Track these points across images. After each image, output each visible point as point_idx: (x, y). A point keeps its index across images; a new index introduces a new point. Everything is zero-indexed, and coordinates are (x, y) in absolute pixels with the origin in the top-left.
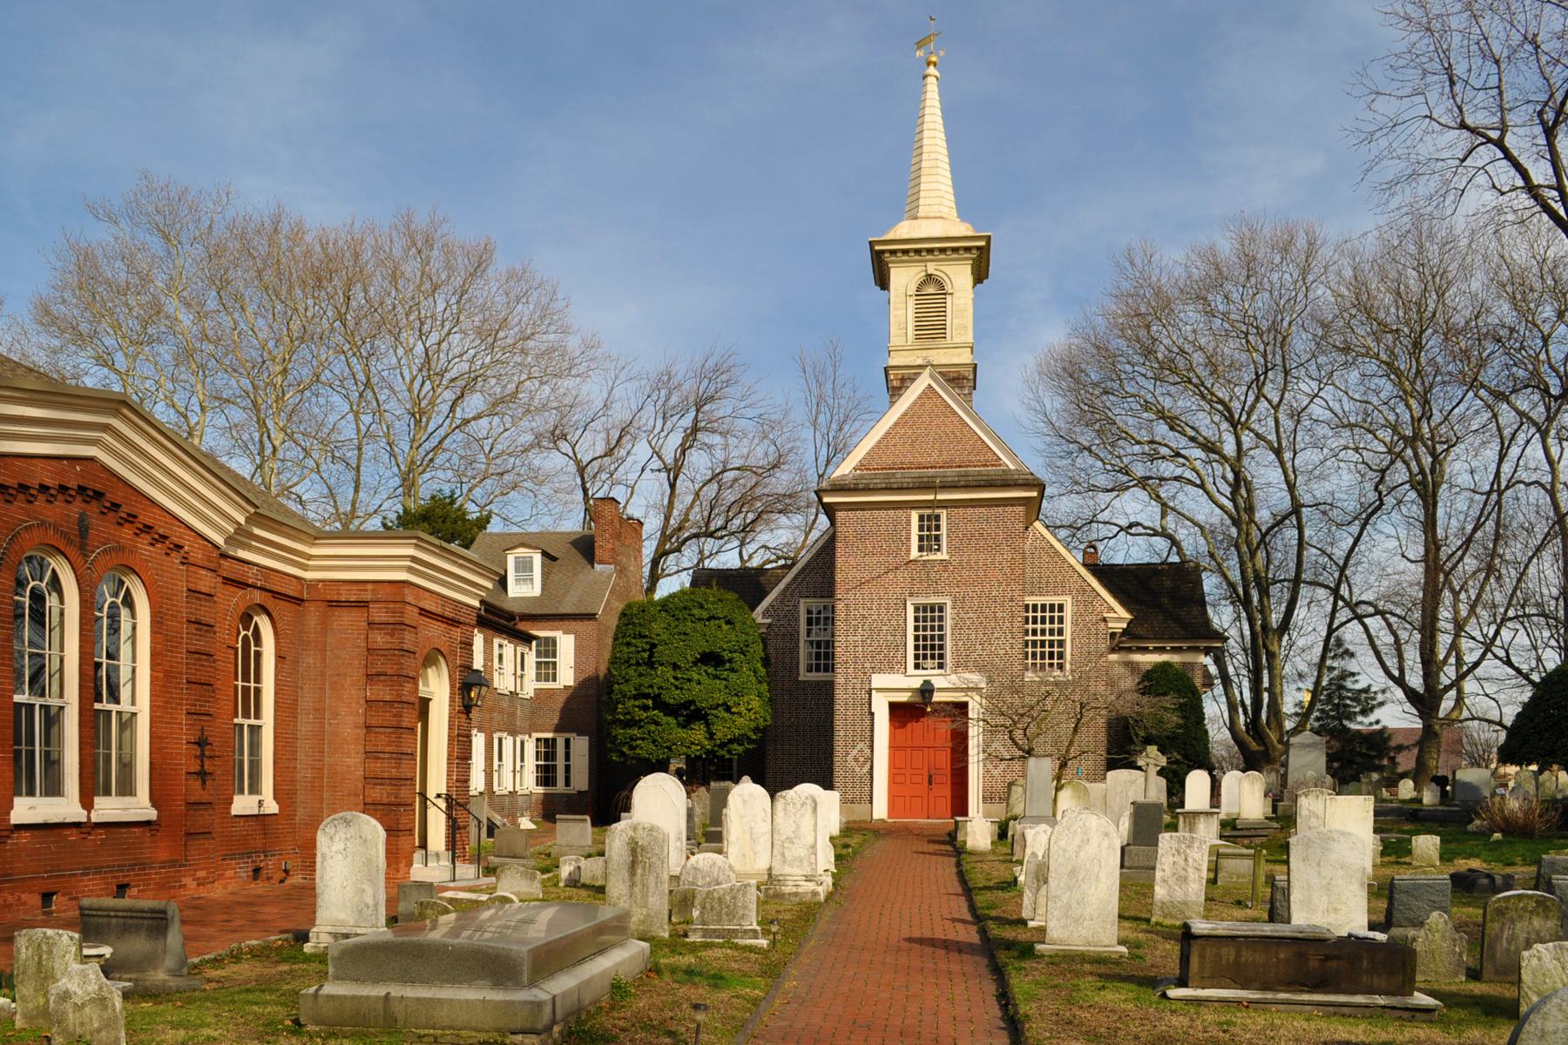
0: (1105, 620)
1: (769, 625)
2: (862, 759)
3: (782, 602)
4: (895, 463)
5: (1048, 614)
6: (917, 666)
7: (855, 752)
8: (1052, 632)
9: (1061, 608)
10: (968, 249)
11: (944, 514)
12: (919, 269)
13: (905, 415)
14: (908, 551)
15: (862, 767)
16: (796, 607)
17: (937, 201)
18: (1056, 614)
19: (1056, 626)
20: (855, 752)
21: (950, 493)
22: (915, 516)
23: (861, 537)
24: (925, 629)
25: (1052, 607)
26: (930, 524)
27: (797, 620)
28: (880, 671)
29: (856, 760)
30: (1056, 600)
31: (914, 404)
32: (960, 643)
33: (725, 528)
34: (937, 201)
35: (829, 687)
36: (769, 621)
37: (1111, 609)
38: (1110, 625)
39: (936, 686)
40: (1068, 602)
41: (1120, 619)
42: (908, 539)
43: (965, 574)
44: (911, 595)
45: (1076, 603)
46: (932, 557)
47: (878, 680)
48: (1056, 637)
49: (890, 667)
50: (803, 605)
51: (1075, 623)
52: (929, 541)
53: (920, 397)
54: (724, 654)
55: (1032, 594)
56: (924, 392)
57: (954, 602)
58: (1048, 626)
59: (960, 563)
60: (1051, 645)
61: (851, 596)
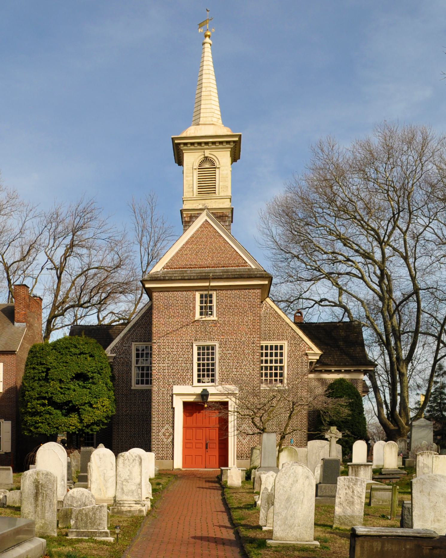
0: (306, 354)
1: (115, 358)
2: (167, 434)
3: (122, 344)
4: (186, 265)
5: (274, 351)
6: (199, 381)
7: (163, 430)
8: (276, 362)
9: (281, 348)
10: (228, 142)
11: (214, 294)
12: (200, 154)
13: (192, 237)
14: (194, 315)
15: (167, 439)
16: (130, 347)
17: (211, 115)
18: (279, 351)
19: (279, 358)
20: (163, 430)
21: (218, 282)
22: (198, 295)
23: (167, 307)
24: (203, 360)
25: (276, 347)
26: (206, 299)
27: (130, 355)
28: (178, 384)
29: (164, 434)
30: (279, 343)
31: (197, 231)
32: (224, 368)
33: (89, 302)
34: (211, 115)
35: (148, 394)
36: (114, 355)
37: (310, 348)
38: (310, 357)
39: (210, 392)
40: (285, 344)
41: (315, 354)
42: (194, 308)
43: (227, 328)
44: (196, 340)
45: (290, 345)
46: (208, 318)
47: (177, 389)
48: (279, 365)
49: (184, 380)
50: (134, 346)
51: (289, 356)
52: (206, 310)
53: (201, 227)
54: (89, 374)
55: (265, 339)
56: (203, 224)
57: (220, 344)
58: (274, 358)
59: (224, 322)
60: (276, 369)
61: (161, 340)
